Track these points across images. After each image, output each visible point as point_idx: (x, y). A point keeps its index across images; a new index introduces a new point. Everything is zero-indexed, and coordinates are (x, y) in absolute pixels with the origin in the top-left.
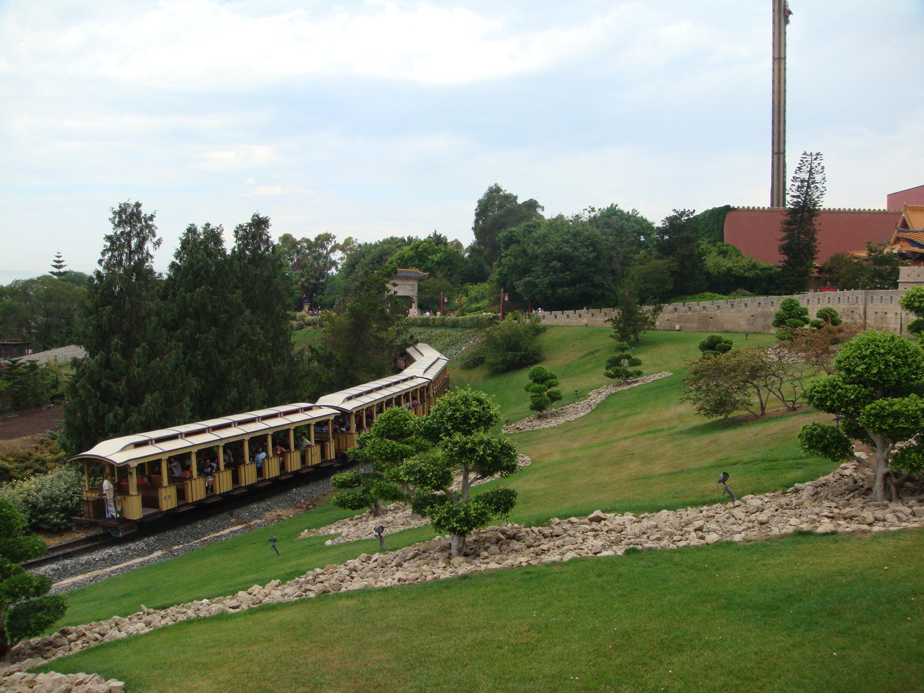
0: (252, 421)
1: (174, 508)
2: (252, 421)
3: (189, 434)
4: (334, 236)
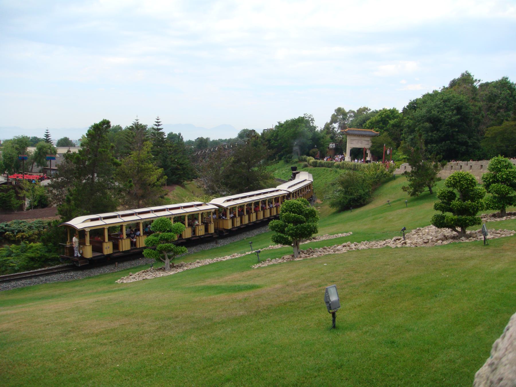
0: (192, 206)
1: (111, 254)
2: (192, 206)
3: (156, 211)
4: (370, 109)
